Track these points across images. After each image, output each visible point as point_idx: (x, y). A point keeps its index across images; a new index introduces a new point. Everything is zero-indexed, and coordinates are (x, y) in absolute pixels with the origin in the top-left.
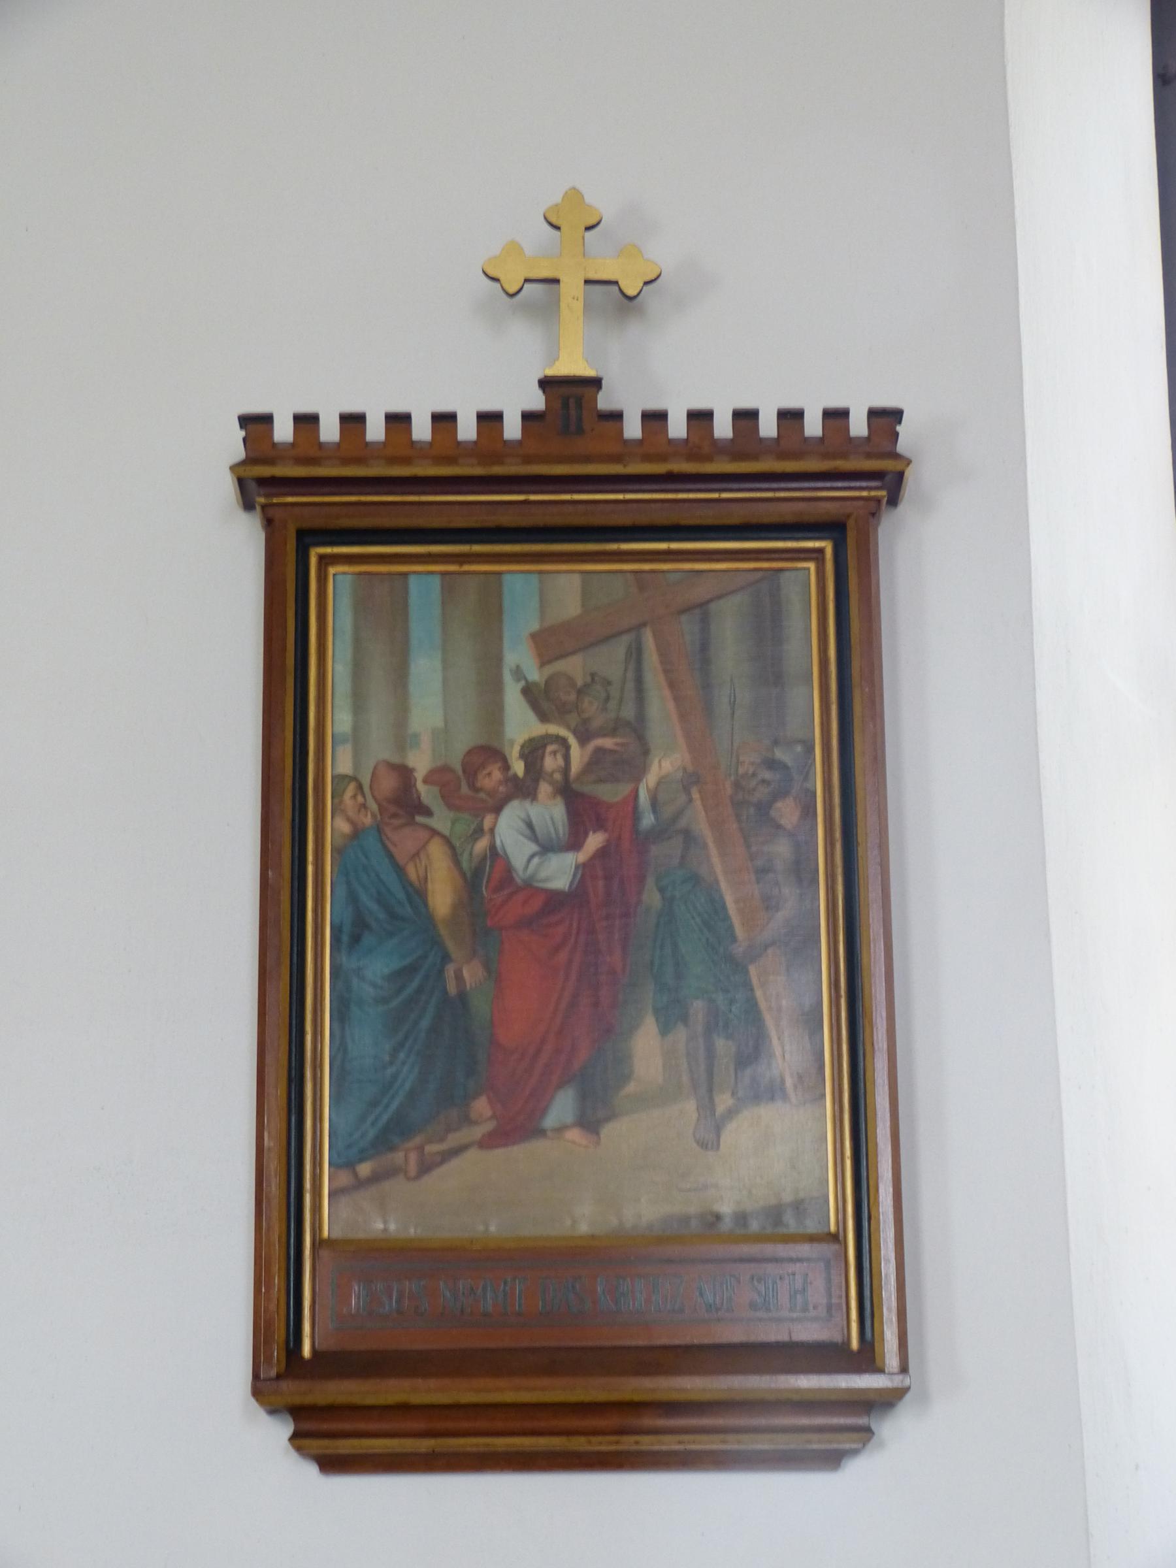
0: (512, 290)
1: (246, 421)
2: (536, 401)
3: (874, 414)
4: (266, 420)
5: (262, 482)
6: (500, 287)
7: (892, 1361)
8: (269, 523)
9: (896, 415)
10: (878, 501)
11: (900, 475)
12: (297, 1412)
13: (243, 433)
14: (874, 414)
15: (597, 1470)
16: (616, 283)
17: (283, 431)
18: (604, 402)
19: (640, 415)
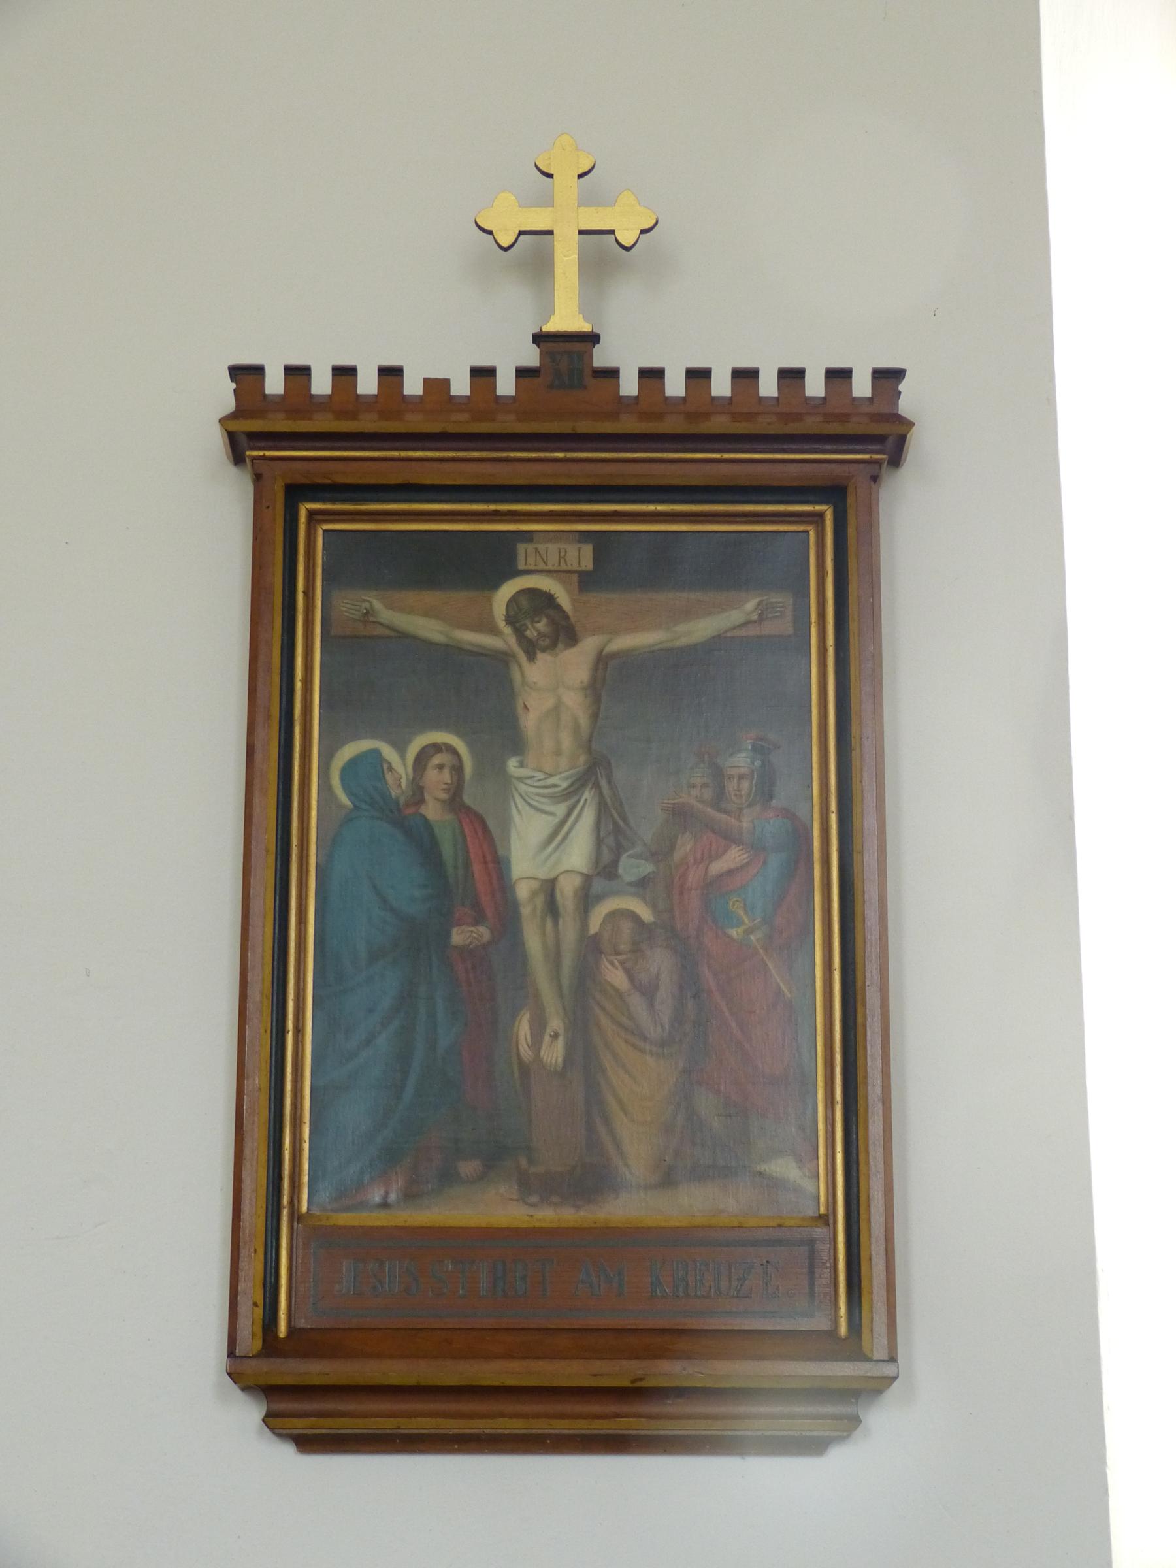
0: (505, 245)
1: (236, 372)
2: (531, 357)
3: (290, 371)
4: (258, 371)
5: (257, 438)
6: (493, 240)
7: (880, 1352)
8: (258, 478)
9: (897, 375)
10: (878, 463)
11: (902, 440)
12: (268, 1391)
13: (234, 385)
14: (290, 371)
15: (577, 1454)
16: (612, 232)
17: (274, 384)
18: (602, 357)
19: (637, 372)
